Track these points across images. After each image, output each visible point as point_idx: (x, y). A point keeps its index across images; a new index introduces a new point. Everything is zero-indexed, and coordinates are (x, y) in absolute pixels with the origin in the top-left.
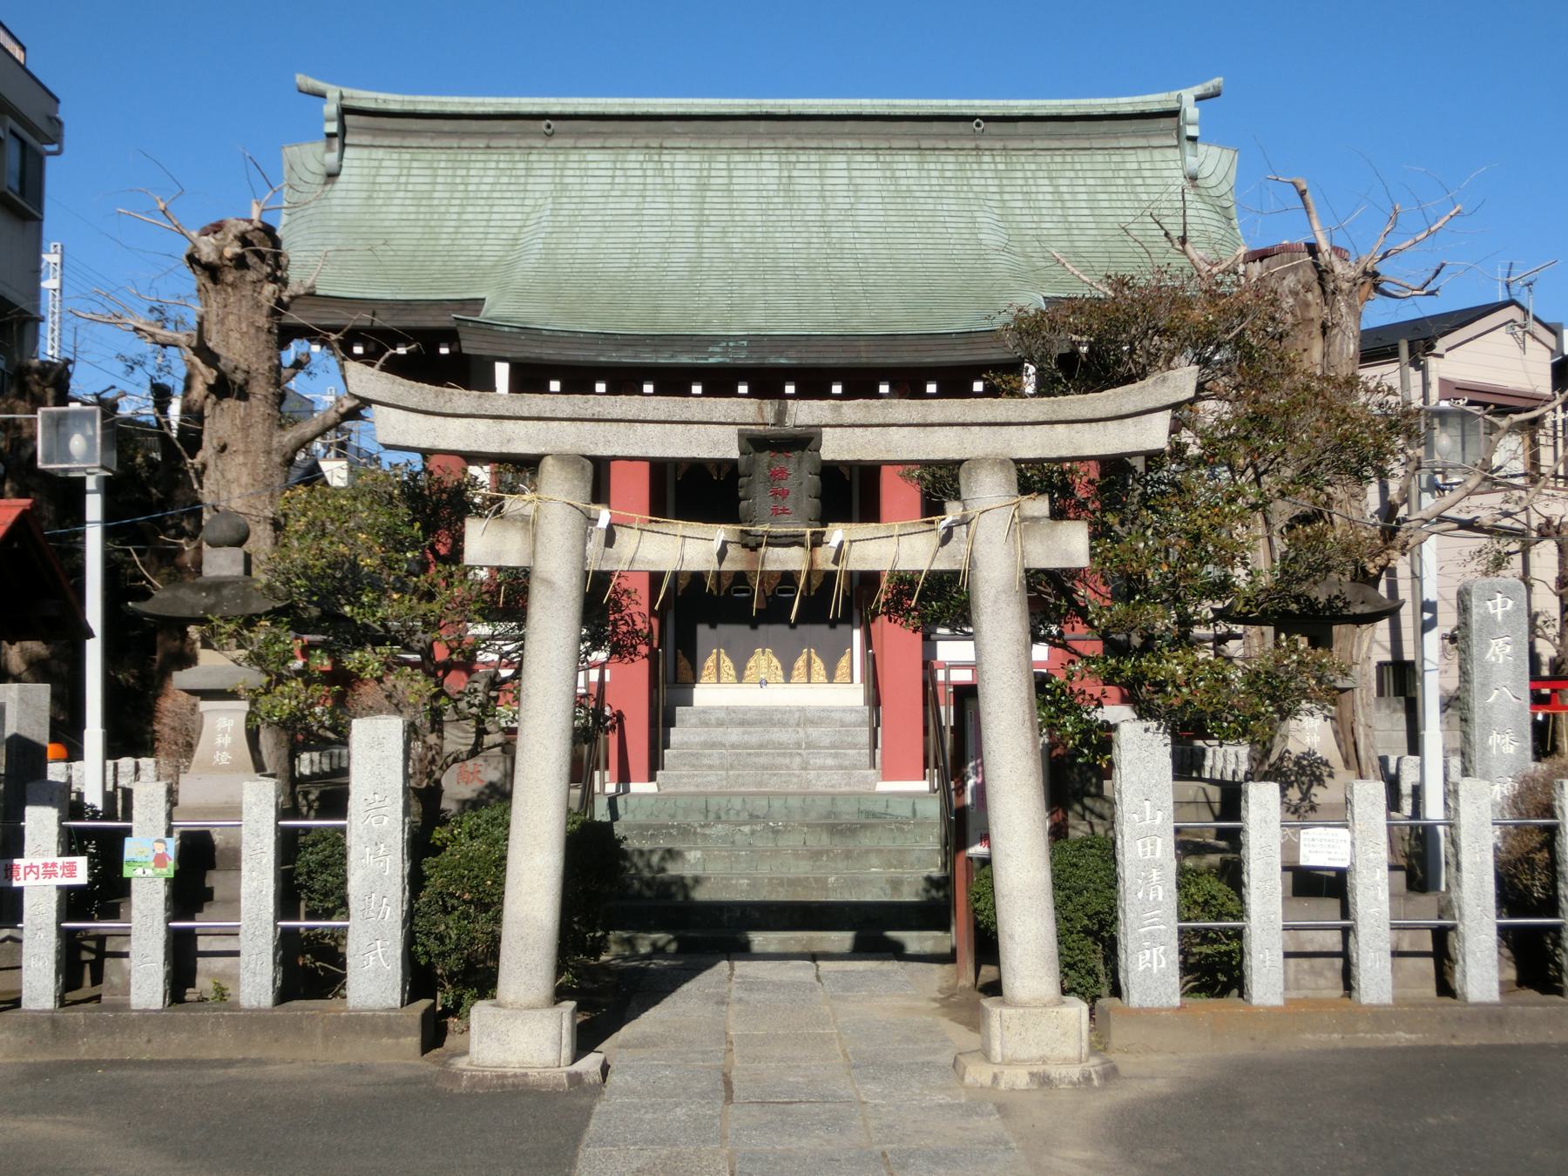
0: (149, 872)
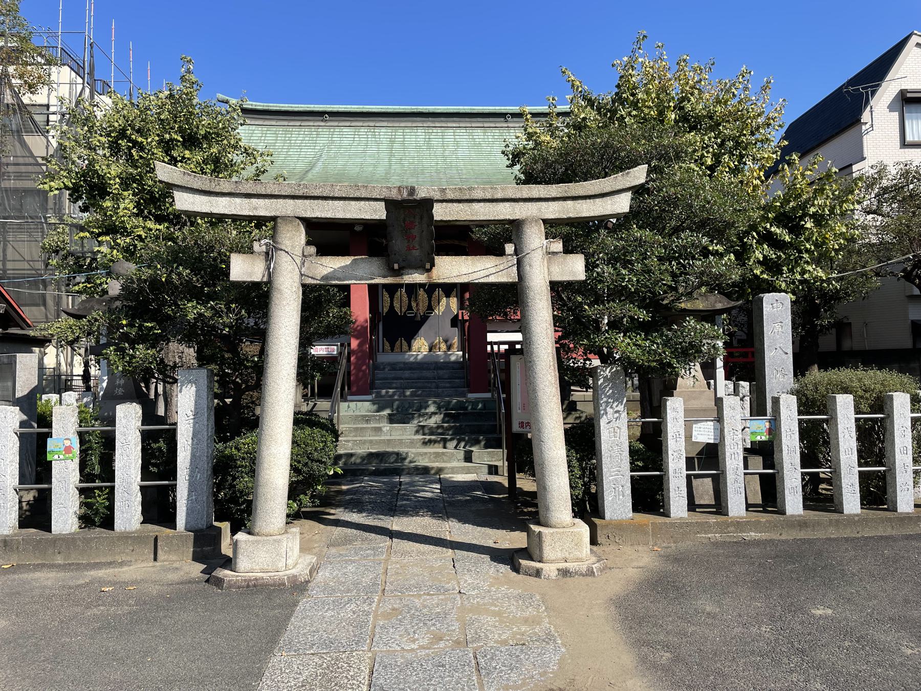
0: (62, 457)
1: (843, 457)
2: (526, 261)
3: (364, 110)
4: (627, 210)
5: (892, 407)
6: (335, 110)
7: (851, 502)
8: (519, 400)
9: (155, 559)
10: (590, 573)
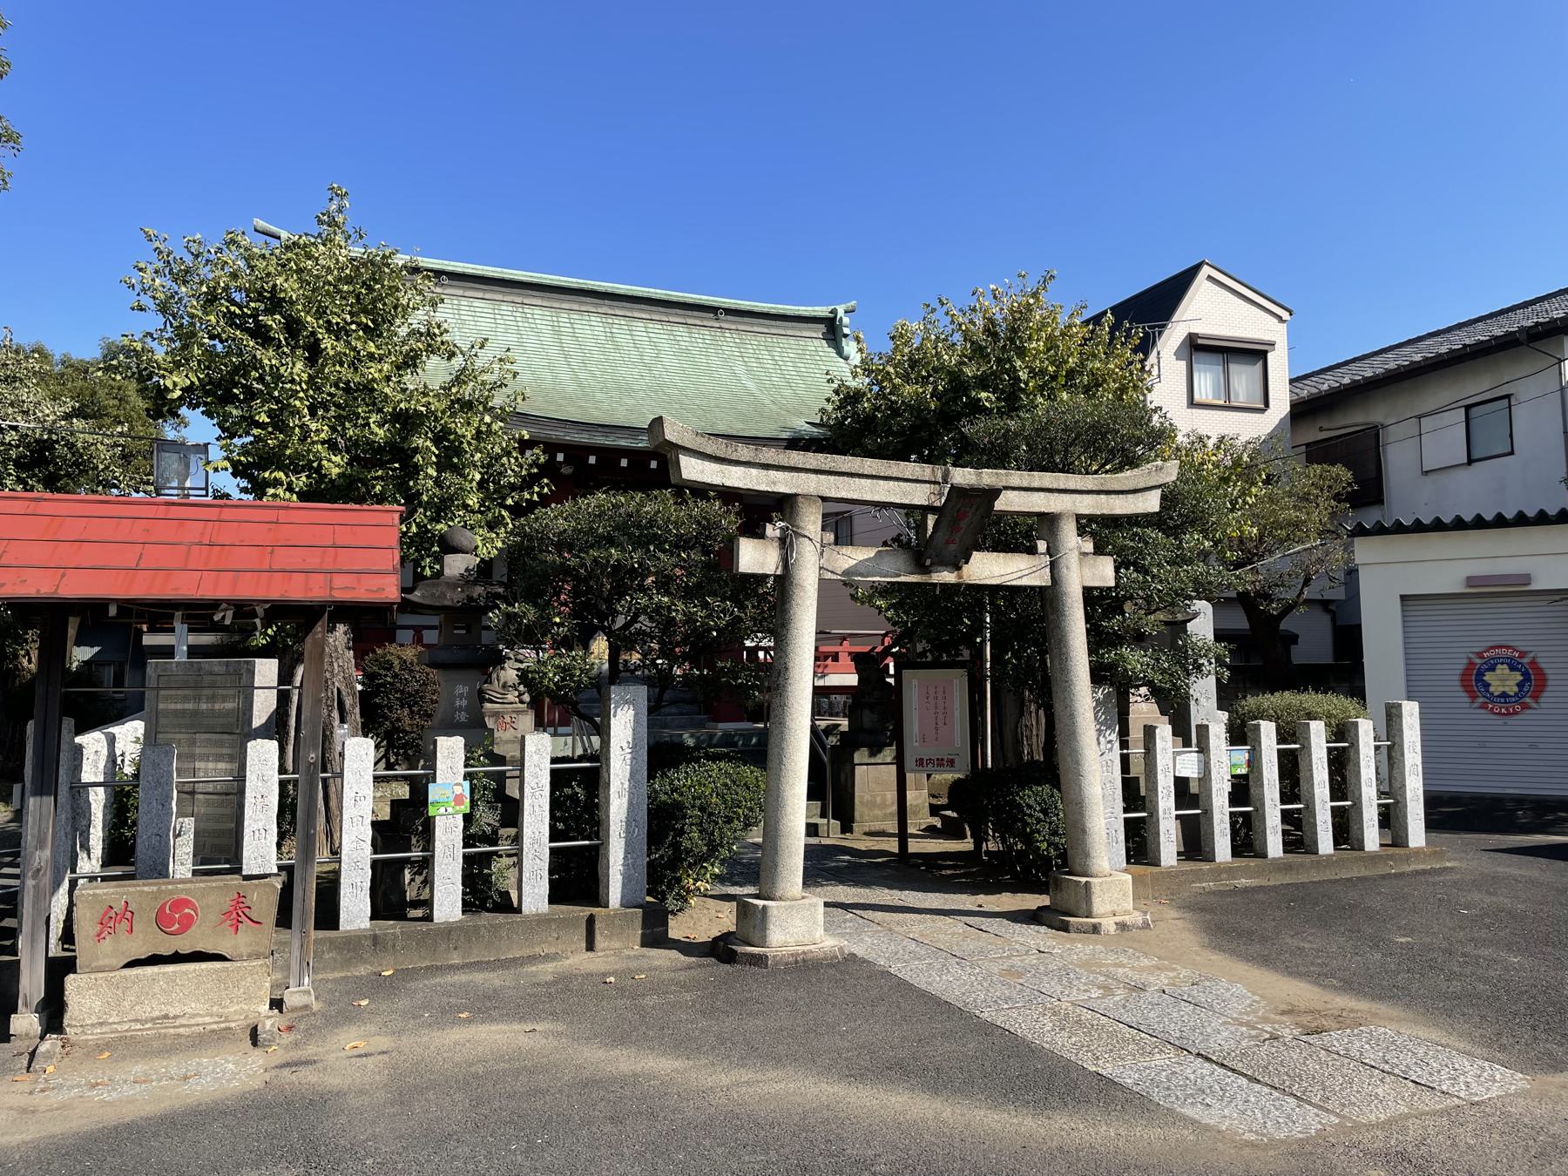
0: (450, 810)
1: (1317, 791)
2: (1063, 562)
3: (506, 276)
4: (1157, 509)
5: (1357, 735)
6: (460, 270)
7: (1325, 844)
8: (916, 729)
9: (590, 946)
10: (1146, 926)
